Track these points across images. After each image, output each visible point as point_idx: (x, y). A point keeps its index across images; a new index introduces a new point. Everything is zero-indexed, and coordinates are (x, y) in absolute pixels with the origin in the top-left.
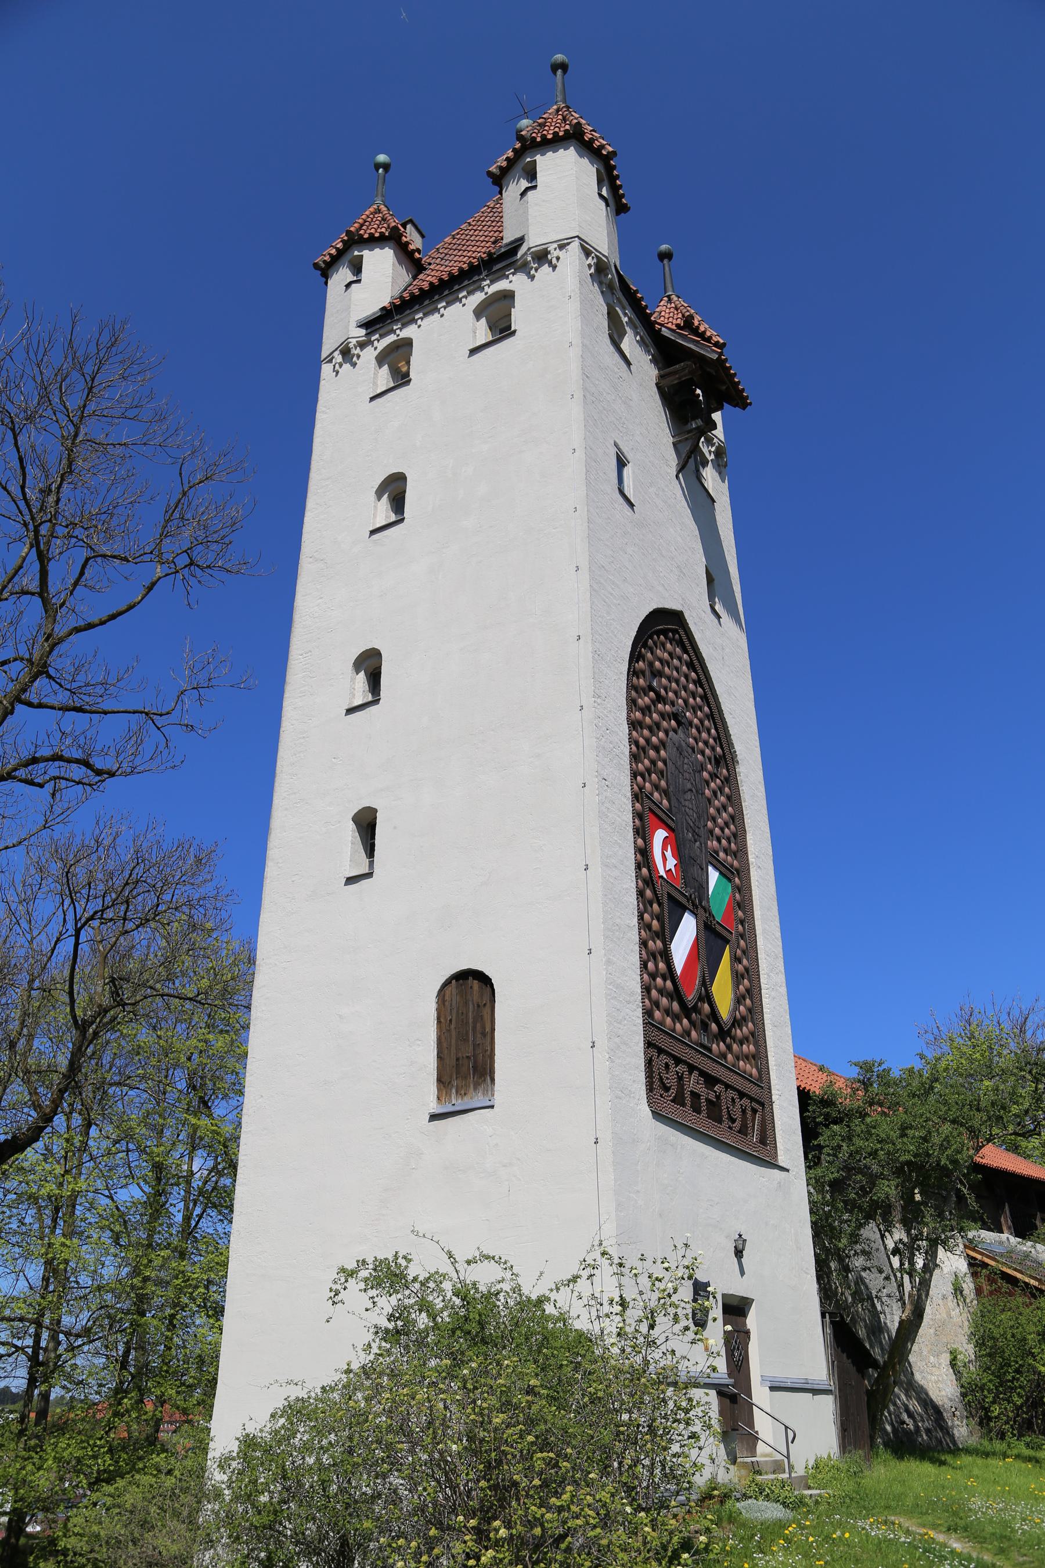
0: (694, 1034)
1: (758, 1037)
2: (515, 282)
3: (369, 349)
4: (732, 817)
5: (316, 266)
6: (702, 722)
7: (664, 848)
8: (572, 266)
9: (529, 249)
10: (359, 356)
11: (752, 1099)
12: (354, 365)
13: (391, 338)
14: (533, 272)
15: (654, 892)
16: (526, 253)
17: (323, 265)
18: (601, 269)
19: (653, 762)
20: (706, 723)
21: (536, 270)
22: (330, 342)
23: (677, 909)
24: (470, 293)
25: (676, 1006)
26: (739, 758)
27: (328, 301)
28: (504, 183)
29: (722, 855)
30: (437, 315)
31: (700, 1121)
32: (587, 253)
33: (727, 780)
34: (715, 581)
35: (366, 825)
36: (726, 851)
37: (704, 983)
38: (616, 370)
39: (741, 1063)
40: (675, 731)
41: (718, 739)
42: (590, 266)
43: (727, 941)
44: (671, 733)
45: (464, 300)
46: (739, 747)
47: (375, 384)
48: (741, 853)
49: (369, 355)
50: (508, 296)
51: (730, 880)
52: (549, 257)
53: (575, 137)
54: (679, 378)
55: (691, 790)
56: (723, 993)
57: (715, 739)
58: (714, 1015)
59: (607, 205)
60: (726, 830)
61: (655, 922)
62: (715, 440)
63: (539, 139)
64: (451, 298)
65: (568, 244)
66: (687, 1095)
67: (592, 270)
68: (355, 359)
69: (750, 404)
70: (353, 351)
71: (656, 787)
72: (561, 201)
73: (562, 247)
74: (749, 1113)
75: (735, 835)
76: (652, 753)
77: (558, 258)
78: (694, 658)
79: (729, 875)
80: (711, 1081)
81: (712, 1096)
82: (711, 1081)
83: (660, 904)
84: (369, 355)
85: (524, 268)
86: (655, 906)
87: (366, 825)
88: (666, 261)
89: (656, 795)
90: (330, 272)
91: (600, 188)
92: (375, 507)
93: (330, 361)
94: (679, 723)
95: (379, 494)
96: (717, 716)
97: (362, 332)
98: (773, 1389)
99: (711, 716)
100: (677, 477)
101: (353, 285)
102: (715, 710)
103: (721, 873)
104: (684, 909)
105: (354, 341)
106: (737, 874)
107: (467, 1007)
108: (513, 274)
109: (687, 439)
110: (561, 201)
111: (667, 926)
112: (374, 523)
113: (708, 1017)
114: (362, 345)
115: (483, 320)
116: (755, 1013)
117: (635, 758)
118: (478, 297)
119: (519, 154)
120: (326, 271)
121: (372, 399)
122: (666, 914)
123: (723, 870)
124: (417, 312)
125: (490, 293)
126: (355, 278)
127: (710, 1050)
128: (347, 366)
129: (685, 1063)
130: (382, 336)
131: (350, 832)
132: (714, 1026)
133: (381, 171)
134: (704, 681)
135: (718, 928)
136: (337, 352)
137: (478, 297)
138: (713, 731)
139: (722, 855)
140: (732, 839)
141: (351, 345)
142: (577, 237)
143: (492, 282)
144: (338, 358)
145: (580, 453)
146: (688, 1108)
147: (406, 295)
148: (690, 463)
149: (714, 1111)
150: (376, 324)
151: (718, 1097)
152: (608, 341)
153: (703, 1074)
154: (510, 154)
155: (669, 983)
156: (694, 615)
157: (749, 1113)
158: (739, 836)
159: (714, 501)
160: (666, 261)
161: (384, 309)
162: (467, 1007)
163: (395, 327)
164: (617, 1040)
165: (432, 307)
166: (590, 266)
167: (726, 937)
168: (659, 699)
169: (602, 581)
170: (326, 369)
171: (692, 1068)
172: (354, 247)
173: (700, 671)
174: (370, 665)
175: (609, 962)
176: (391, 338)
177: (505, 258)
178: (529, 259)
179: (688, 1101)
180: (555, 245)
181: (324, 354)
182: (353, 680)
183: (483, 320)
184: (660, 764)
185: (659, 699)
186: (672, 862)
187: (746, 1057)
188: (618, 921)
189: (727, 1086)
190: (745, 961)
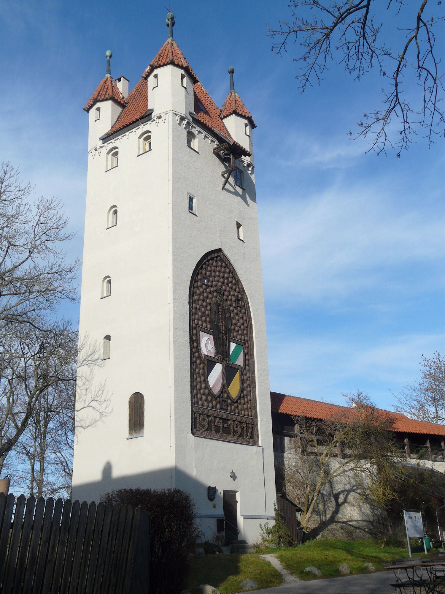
15: (201, 360)
22: (90, 147)
47: (107, 165)
58: (229, 397)
66: (213, 427)
74: (245, 430)
80: (225, 420)
81: (226, 425)
107: (137, 404)
122: (206, 367)
145: (171, 205)
150: (106, 138)
153: (221, 418)
162: (137, 404)
170: (90, 156)
176: (111, 146)
177: (147, 116)
179: (213, 429)
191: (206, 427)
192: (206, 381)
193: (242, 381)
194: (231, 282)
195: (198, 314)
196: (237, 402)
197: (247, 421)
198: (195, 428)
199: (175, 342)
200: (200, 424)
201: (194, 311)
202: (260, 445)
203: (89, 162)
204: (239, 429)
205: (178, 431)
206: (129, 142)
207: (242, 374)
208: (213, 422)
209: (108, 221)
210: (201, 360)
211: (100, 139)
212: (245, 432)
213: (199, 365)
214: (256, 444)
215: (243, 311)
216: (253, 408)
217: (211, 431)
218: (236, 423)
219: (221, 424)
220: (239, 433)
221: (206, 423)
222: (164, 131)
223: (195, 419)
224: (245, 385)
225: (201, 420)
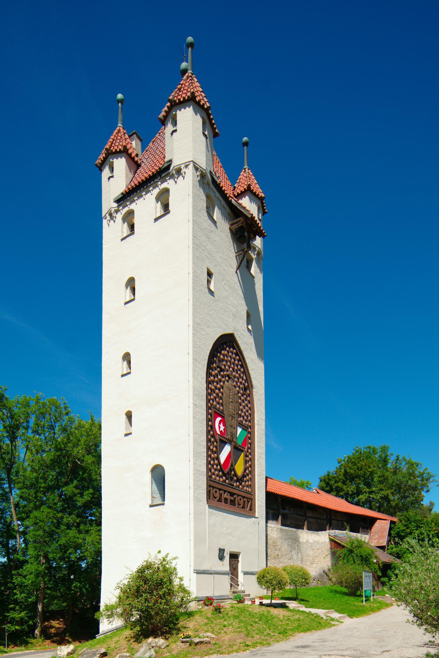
0: (227, 481)
1: (252, 479)
2: (169, 184)
3: (119, 213)
4: (250, 408)
5: (96, 165)
6: (240, 375)
7: (220, 423)
8: (190, 177)
9: (174, 167)
10: (116, 217)
11: (247, 498)
12: (114, 221)
13: (126, 209)
14: (176, 179)
15: (215, 439)
16: (173, 170)
17: (99, 165)
18: (203, 176)
19: (218, 395)
20: (242, 375)
21: (177, 178)
22: (105, 211)
23: (223, 443)
24: (154, 188)
25: (221, 473)
26: (254, 386)
27: (103, 185)
28: (165, 123)
29: (244, 422)
30: (142, 199)
31: (228, 506)
32: (196, 169)
33: (249, 395)
34: (250, 317)
35: (129, 415)
36: (246, 421)
37: (232, 465)
38: (209, 228)
39: (245, 488)
40: (228, 381)
41: (246, 381)
42: (198, 176)
43: (242, 451)
44: (226, 382)
45: (151, 191)
46: (254, 382)
47: (122, 232)
48: (252, 420)
49: (119, 217)
50: (167, 191)
51: (246, 430)
52: (182, 172)
53: (191, 100)
54: (238, 225)
55: (232, 402)
56: (239, 468)
57: (245, 381)
58: (235, 475)
59: (207, 138)
60: (247, 413)
61: (214, 449)
62: (257, 248)
63: (177, 101)
64: (147, 190)
65: (189, 165)
66: (223, 499)
67: (199, 178)
68: (114, 219)
69: (266, 236)
70: (113, 215)
71: (218, 403)
72: (186, 140)
73: (186, 166)
74: (246, 502)
75: (250, 415)
76: (217, 391)
77: (185, 173)
78: (238, 351)
79: (246, 429)
80: (232, 494)
81: (232, 498)
82: (232, 494)
83: (217, 443)
84: (119, 217)
85: (172, 177)
86: (215, 443)
87: (129, 415)
88: (245, 147)
89: (218, 406)
90: (102, 168)
91: (204, 130)
92: (126, 292)
93: (105, 219)
94: (230, 378)
95: (127, 286)
96: (246, 372)
97: (116, 205)
98: (197, 573)
99: (244, 372)
100: (236, 272)
101: (111, 179)
102: (246, 370)
103: (243, 429)
104: (225, 443)
105: (113, 209)
106: (249, 428)
107: (158, 475)
108: (169, 179)
109: (240, 254)
110: (186, 140)
111: (218, 449)
112: (125, 299)
113: (233, 475)
114: (117, 211)
115: (159, 203)
116: (252, 472)
117: (208, 394)
118: (156, 191)
119: (170, 108)
120: (100, 168)
121: (122, 240)
123: (243, 427)
124: (135, 197)
125: (161, 189)
126: (111, 175)
127: (233, 485)
128: (112, 221)
129: (223, 490)
130: (124, 207)
131: (124, 418)
132: (235, 478)
133: (120, 104)
134: (242, 359)
135: (239, 447)
136: (107, 215)
137: (156, 191)
138: (245, 378)
139: (244, 422)
140: (249, 416)
141: (112, 212)
142: (192, 161)
143: (162, 183)
144: (108, 218)
145: (191, 275)
146: (223, 503)
147: (130, 187)
148: (244, 264)
149: (233, 503)
150: (124, 199)
151: (235, 499)
152: (206, 214)
153: (229, 492)
154: (166, 109)
155: (219, 467)
156: (239, 333)
157: (246, 502)
158: (252, 415)
159: (254, 277)
160: (245, 147)
161: (122, 193)
162: (158, 475)
163: (128, 203)
164: (197, 486)
165: (140, 195)
166: (198, 176)
167: (244, 449)
168: (222, 370)
169: (198, 330)
170: (105, 222)
171: (225, 491)
172: (110, 156)
173: (240, 356)
174: (127, 358)
175: (194, 464)
176: (126, 209)
177: (164, 172)
178: (174, 172)
179: (223, 500)
180: (183, 166)
181: (103, 215)
182: (122, 364)
183: (159, 203)
184: (220, 394)
185: (222, 370)
186: (222, 428)
187: (248, 486)
188: (199, 451)
189: (238, 495)
190: (250, 456)
191: (218, 499)
192: (218, 459)
193: (246, 462)
194: (240, 370)
195: (213, 395)
196: (241, 479)
197: (249, 496)
198: (209, 499)
199: (194, 417)
200: (213, 496)
201: (209, 391)
202: (257, 516)
203: (104, 229)
204: (242, 502)
205: (196, 500)
206: (145, 206)
207: (246, 456)
208: (223, 495)
209: (126, 296)
210: (215, 439)
211: (115, 202)
212: (246, 505)
213: (214, 442)
214: (253, 516)
215: (248, 398)
216: (252, 486)
217: (221, 502)
218: (239, 497)
219: (229, 497)
220: (241, 506)
221: (217, 495)
222: (184, 191)
223: (210, 491)
224: (248, 465)
225: (214, 492)
